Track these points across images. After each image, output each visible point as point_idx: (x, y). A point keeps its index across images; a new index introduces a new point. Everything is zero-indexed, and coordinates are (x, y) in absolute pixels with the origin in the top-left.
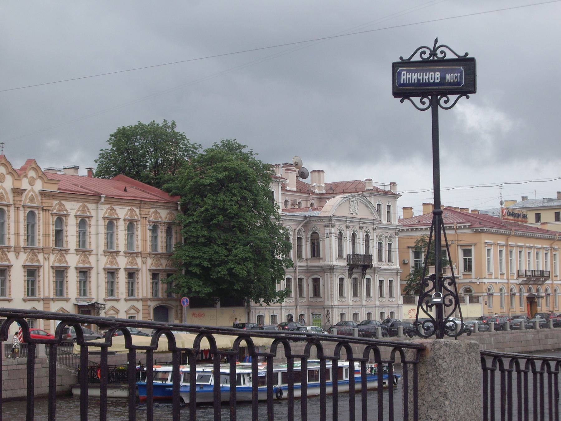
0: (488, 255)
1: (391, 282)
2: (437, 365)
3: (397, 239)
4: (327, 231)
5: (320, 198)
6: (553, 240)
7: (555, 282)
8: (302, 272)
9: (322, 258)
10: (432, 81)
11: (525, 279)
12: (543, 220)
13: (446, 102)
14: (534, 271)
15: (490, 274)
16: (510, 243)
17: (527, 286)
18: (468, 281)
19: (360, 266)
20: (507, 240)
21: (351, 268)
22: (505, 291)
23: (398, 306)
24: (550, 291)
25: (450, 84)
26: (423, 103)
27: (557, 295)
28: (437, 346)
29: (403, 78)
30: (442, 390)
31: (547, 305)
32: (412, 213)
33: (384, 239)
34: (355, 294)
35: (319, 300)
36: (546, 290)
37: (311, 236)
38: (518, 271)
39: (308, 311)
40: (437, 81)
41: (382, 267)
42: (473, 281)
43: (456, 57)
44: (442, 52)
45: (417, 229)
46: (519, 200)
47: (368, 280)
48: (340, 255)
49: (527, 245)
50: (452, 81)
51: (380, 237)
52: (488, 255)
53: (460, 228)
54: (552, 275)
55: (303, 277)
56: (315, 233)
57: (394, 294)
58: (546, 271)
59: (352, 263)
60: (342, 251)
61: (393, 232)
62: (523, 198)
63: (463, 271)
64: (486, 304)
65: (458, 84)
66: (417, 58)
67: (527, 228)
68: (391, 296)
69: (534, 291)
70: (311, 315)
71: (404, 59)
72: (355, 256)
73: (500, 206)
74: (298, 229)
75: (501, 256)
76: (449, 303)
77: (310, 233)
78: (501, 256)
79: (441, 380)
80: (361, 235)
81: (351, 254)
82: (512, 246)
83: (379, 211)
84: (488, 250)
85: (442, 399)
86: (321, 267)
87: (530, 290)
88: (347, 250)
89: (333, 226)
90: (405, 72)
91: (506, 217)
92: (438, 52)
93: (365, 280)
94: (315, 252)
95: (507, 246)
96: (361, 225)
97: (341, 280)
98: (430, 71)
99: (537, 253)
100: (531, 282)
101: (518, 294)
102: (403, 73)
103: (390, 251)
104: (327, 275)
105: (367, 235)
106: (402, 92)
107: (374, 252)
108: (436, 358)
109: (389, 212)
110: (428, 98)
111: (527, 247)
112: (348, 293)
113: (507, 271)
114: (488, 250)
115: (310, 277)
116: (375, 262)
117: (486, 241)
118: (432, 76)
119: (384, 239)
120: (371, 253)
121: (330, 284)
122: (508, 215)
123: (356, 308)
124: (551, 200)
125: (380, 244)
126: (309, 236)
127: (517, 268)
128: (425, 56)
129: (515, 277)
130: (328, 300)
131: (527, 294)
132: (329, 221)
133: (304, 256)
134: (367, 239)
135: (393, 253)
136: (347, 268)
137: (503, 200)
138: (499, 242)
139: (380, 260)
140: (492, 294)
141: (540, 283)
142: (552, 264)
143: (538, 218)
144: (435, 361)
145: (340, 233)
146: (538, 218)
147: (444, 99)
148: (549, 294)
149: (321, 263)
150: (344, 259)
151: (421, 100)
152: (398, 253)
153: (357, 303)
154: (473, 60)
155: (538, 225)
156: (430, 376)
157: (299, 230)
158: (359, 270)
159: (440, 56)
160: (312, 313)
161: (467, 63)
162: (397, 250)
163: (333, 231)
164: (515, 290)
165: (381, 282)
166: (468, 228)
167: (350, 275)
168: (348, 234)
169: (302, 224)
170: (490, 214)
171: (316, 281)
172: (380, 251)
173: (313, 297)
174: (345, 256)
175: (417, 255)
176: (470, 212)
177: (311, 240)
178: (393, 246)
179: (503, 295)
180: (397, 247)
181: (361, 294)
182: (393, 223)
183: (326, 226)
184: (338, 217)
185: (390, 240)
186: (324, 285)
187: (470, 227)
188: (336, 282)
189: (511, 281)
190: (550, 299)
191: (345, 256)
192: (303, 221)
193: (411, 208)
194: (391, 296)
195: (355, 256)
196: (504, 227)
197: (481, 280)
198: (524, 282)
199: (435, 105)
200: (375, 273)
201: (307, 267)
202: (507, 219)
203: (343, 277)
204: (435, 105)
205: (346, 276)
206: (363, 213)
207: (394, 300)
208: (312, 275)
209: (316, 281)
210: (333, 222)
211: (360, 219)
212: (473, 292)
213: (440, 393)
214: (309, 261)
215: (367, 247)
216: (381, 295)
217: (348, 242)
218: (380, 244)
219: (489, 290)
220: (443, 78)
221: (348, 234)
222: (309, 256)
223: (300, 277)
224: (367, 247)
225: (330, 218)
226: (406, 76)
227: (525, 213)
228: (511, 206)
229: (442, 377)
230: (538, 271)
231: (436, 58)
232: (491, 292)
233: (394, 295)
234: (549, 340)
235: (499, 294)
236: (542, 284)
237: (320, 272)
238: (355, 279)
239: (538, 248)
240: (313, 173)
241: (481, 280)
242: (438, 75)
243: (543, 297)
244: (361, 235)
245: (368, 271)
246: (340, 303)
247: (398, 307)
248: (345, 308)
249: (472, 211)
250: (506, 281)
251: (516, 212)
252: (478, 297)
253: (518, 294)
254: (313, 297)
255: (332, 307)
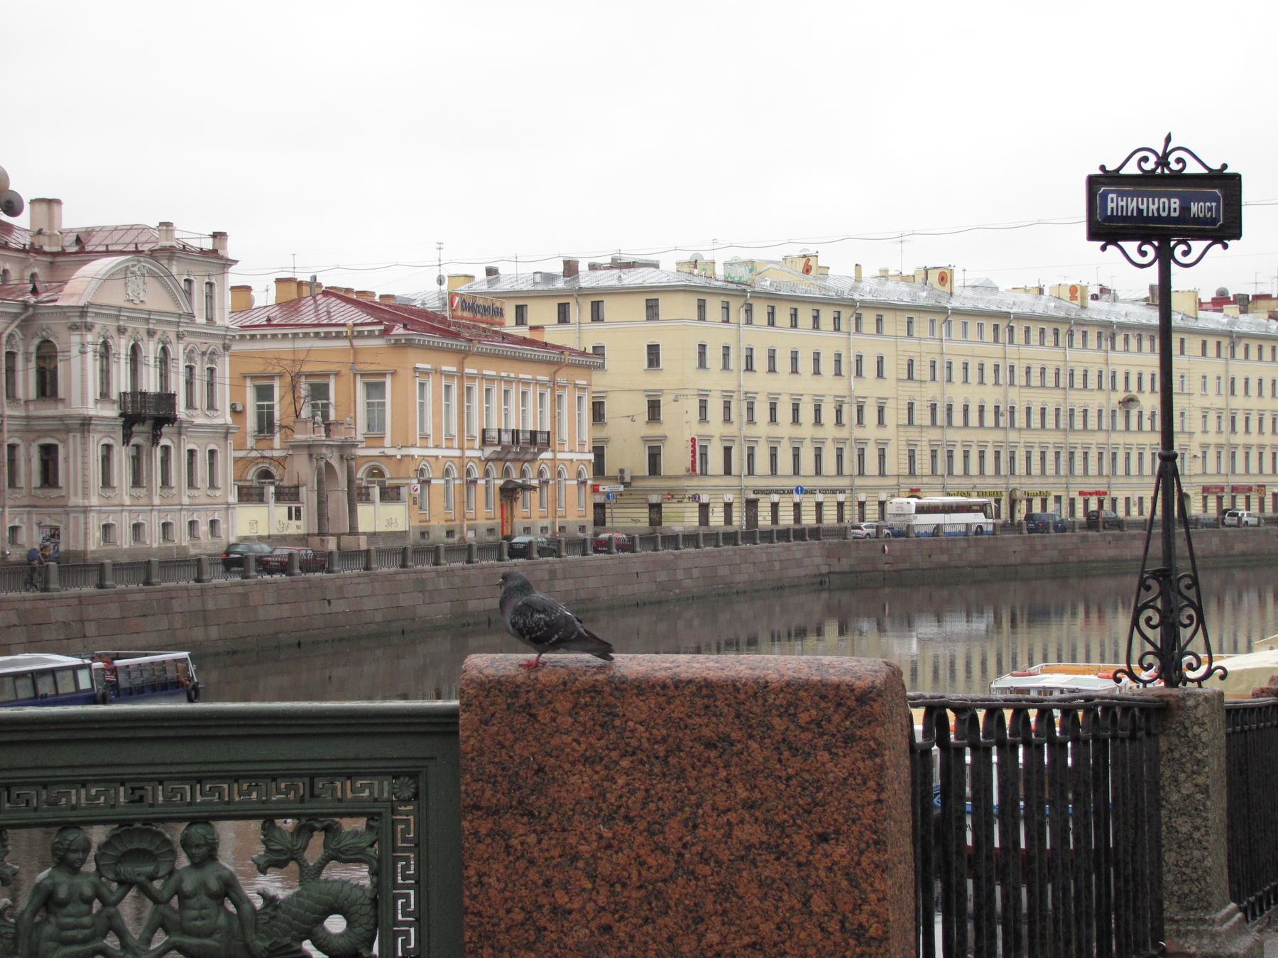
0: (422, 396)
1: (212, 453)
2: (1190, 735)
3: (227, 359)
4: (75, 338)
5: (52, 263)
6: (558, 365)
7: (559, 456)
8: (16, 431)
9: (62, 400)
10: (1164, 214)
11: (499, 449)
12: (532, 320)
13: (1185, 253)
14: (515, 433)
15: (425, 437)
16: (467, 370)
17: (500, 464)
18: (375, 452)
19: (148, 417)
20: (461, 366)
21: (129, 421)
22: (455, 473)
23: (228, 506)
24: (548, 475)
25: (1197, 220)
26: (1144, 254)
27: (563, 483)
28: (1190, 702)
29: (1110, 205)
30: (1200, 780)
31: (541, 506)
32: (250, 301)
33: (198, 359)
34: (137, 483)
35: (54, 493)
36: (541, 473)
37: (39, 348)
38: (484, 431)
39: (30, 519)
40: (1173, 214)
41: (198, 421)
42: (389, 452)
43: (1206, 172)
44: (1179, 160)
45: (264, 336)
46: (481, 275)
47: (166, 449)
48: (105, 395)
49: (503, 374)
50: (1201, 215)
51: (190, 355)
52: (422, 396)
53: (360, 335)
54: (555, 441)
55: (17, 441)
56: (46, 342)
57: (220, 482)
58: (541, 432)
59: (129, 411)
60: (108, 384)
61: (216, 344)
62: (491, 272)
63: (365, 431)
64: (415, 503)
65: (1213, 221)
66: (1131, 169)
67: (505, 337)
68: (212, 485)
69: (515, 475)
70: (35, 528)
71: (1108, 168)
72: (137, 395)
73: (436, 287)
74: (8, 332)
75: (447, 398)
76: (1187, 622)
77: (37, 341)
78: (447, 398)
79: (1198, 762)
80: (150, 350)
81: (129, 390)
82: (472, 377)
83: (189, 294)
84: (422, 385)
85: (1199, 796)
86: (61, 418)
87: (506, 472)
88: (120, 382)
89: (89, 328)
90: (1114, 196)
91: (459, 313)
92: (1172, 159)
93: (159, 449)
94: (47, 386)
95: (462, 376)
96: (151, 326)
97: (108, 448)
98: (1160, 196)
99: (524, 394)
100: (510, 456)
101: (483, 482)
102: (1110, 196)
103: (211, 385)
104: (74, 440)
105: (164, 350)
106: (1105, 229)
107: (177, 385)
108: (1187, 723)
109: (210, 297)
110: (1153, 246)
111: (502, 379)
112: (121, 480)
113: (461, 431)
114: (422, 385)
115: (34, 441)
116: (181, 411)
117: (418, 365)
118: (1167, 205)
119: (198, 359)
120: (172, 389)
121: (81, 461)
122: (463, 310)
123: (139, 512)
124: (549, 278)
125: (190, 369)
126: (33, 349)
127: (481, 423)
128: (1149, 166)
129: (477, 443)
130: (76, 494)
131: (501, 482)
132: (81, 318)
133: (20, 393)
134: (164, 359)
135: (218, 388)
136: (120, 422)
137: (445, 274)
138: (444, 368)
139: (190, 405)
140: (428, 482)
141: (528, 457)
142: (553, 417)
143: (521, 313)
144: (1186, 729)
145: (105, 345)
146: (521, 313)
147: (1182, 247)
148: (546, 482)
149: (60, 410)
150: (114, 402)
151: (1140, 247)
152: (228, 387)
153: (142, 501)
154: (1236, 178)
155: (523, 332)
156: (1177, 755)
157: (11, 336)
158: (146, 428)
159: (1175, 167)
160: (39, 524)
161: (1226, 184)
162: (227, 381)
163: (90, 337)
164: (476, 474)
165: (191, 453)
166: (376, 337)
167: (127, 438)
168: (122, 346)
169: (17, 322)
170: (418, 304)
171: (49, 453)
172: (190, 384)
173: (42, 487)
174: (114, 395)
175: (264, 393)
176: (377, 299)
177: (38, 358)
178: (218, 373)
179: (452, 483)
180: (227, 375)
181: (150, 482)
182: (219, 322)
183: (74, 328)
184: (101, 306)
185: (212, 361)
186: (66, 459)
187: (386, 332)
188: (95, 453)
189: (468, 453)
190: (548, 492)
191: (114, 395)
192: (21, 314)
193: (248, 289)
194: (212, 485)
195: (137, 395)
196: (456, 336)
197: (405, 452)
198: (494, 456)
199: (1165, 257)
200: (180, 434)
201: (28, 418)
202: (462, 318)
203: (111, 441)
204: (1165, 257)
205: (116, 440)
206: (154, 298)
207: (218, 493)
208: (39, 438)
209: (49, 453)
210: (89, 320)
211: (150, 312)
212: (388, 475)
213: (1196, 785)
214: (31, 407)
215: (164, 377)
216: (191, 484)
217: (123, 362)
218: (190, 369)
219: (422, 472)
220: (1185, 209)
221: (122, 346)
222: (33, 393)
223: (11, 441)
224: (164, 377)
225: (83, 311)
226: (1115, 203)
227: (498, 305)
228: (463, 289)
229: (1199, 756)
230: (524, 431)
231: (1166, 171)
232: (425, 478)
233: (220, 483)
234: (557, 582)
235: (443, 482)
236: (533, 460)
237: (57, 431)
238: (138, 447)
239: (526, 383)
240: (37, 205)
241: (405, 452)
242: (1175, 203)
243: (534, 488)
244: (150, 350)
245: (166, 429)
246: (104, 501)
247: (227, 509)
248: (114, 512)
249: (381, 297)
250: (457, 453)
251: (480, 302)
252: (398, 487)
253: (481, 482)
254: (42, 487)
255: (86, 510)
